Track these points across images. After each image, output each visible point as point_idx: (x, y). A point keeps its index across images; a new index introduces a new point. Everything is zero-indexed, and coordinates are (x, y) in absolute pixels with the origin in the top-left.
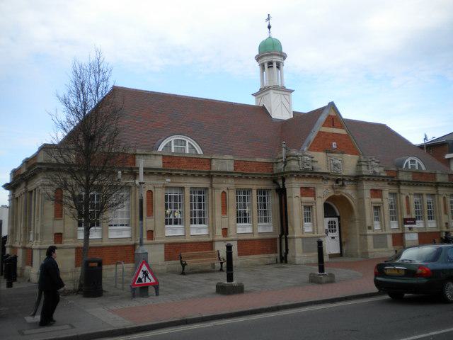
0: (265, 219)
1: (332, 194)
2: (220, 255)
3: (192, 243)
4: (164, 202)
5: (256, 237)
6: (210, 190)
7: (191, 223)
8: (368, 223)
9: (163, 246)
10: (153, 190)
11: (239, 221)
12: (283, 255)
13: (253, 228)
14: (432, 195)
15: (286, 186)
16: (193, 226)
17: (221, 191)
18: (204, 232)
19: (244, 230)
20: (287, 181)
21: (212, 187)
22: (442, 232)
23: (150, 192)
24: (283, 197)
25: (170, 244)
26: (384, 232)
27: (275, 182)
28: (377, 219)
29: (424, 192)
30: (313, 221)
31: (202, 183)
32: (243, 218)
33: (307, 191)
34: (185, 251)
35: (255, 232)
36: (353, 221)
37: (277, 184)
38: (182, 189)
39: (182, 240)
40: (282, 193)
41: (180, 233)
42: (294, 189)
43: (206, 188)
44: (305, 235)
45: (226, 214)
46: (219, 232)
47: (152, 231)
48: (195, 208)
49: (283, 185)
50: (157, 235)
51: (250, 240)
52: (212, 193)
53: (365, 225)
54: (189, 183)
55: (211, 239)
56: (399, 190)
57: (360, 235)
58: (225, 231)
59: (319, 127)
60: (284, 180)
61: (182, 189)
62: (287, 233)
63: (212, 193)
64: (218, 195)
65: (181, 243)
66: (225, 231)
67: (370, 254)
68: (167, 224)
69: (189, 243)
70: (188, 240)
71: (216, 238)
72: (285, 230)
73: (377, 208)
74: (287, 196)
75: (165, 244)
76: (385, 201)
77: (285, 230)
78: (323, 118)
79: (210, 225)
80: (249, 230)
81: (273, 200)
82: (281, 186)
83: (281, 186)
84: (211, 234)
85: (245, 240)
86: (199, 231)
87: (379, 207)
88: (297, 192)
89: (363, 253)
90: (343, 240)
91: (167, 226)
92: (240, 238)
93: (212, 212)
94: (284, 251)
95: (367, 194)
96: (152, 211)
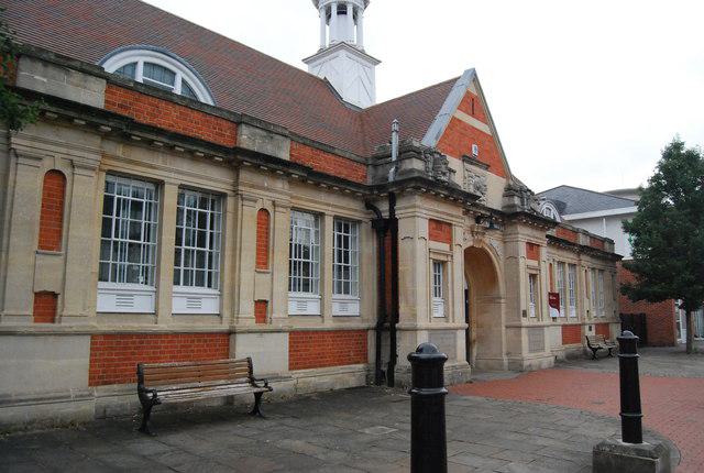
0: (200, 276)
1: (470, 244)
2: (256, 371)
3: (176, 334)
4: (99, 215)
5: (329, 324)
6: (230, 201)
7: (177, 282)
8: (523, 308)
9: (86, 342)
10: (67, 172)
11: (293, 286)
12: (384, 369)
13: (322, 306)
14: (573, 266)
15: (398, 214)
16: (181, 288)
17: (259, 206)
18: (209, 306)
19: (300, 308)
20: (399, 204)
21: (236, 193)
22: (584, 324)
23: (55, 175)
24: (388, 241)
25: (108, 336)
26: (450, 325)
27: (370, 206)
28: (437, 293)
29: (330, 212)
30: (222, 286)
31: (213, 178)
32: (302, 274)
33: (440, 228)
34: (156, 359)
35: (326, 314)
36: (495, 300)
37: (376, 211)
38: (159, 184)
39: (147, 326)
40: (386, 231)
41: (142, 304)
42: (416, 218)
43: (221, 196)
44: (434, 325)
45: (265, 264)
46: (247, 309)
47: (54, 295)
48: (117, 236)
49: (392, 211)
50: (70, 306)
51: (316, 332)
52: (236, 210)
53: (518, 308)
54: (178, 173)
55: (225, 327)
56: (236, 184)
57: (507, 327)
58: (262, 307)
59: (450, 107)
60: (392, 200)
61: (159, 184)
62: (396, 318)
63: (236, 210)
64: (249, 214)
65: (142, 336)
66: (262, 307)
67: (236, 403)
68: (103, 278)
69: (166, 335)
70: (164, 326)
71: (240, 325)
72: (389, 310)
73: (533, 277)
74: (401, 234)
75: (93, 336)
76: (542, 264)
77: (389, 310)
78: (456, 96)
79: (226, 291)
80: (313, 308)
81: (364, 247)
82: (386, 215)
83: (386, 215)
84: (226, 314)
85: (306, 332)
86: (191, 306)
87: (444, 263)
88: (423, 228)
89: (512, 363)
90: (474, 335)
91: (102, 285)
92: (298, 326)
93: (234, 256)
94: (386, 358)
95: (523, 250)
96: (60, 233)
